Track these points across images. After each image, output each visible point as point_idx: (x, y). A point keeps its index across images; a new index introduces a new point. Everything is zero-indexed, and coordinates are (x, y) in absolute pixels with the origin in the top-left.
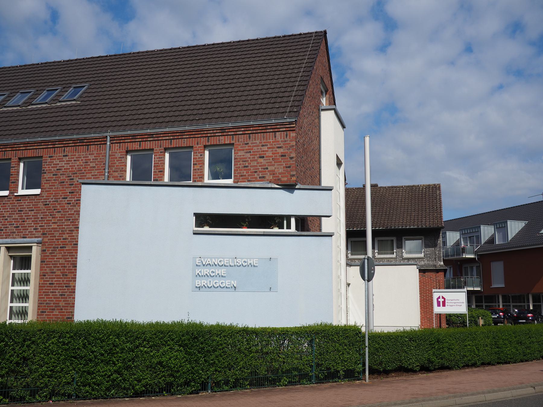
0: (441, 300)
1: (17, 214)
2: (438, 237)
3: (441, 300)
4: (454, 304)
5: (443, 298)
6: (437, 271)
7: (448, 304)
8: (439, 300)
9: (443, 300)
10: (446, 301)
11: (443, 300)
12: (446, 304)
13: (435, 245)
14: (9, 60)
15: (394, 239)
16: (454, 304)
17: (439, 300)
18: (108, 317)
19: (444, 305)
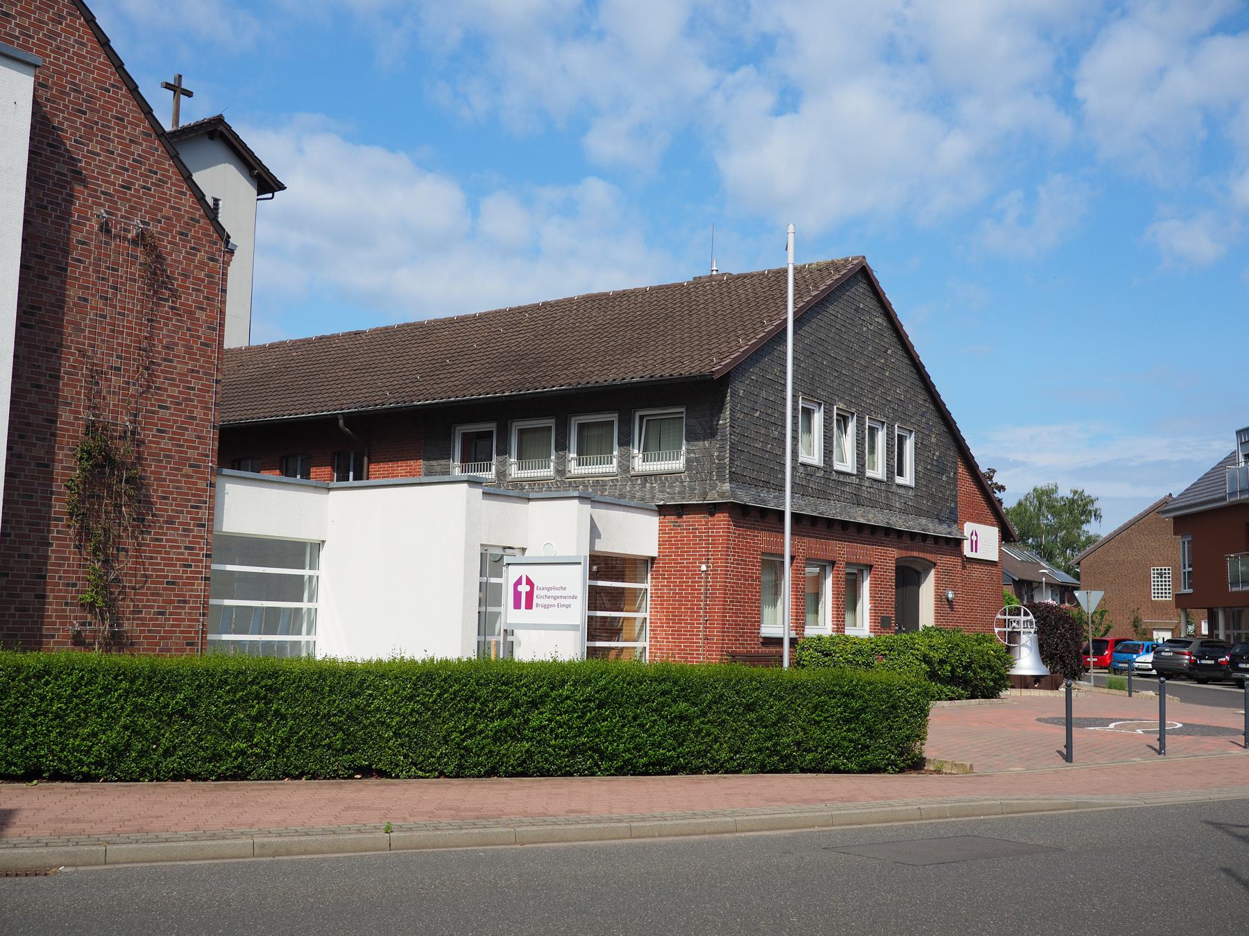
0: (524, 588)
1: (188, 512)
2: (721, 409)
3: (524, 588)
4: (551, 601)
5: (529, 582)
6: (712, 509)
7: (540, 601)
8: (520, 588)
9: (528, 588)
10: (536, 593)
11: (528, 588)
12: (535, 601)
13: (711, 432)
14: (3, 807)
15: (614, 417)
16: (551, 601)
17: (520, 588)
18: (382, 325)
19: (529, 606)
